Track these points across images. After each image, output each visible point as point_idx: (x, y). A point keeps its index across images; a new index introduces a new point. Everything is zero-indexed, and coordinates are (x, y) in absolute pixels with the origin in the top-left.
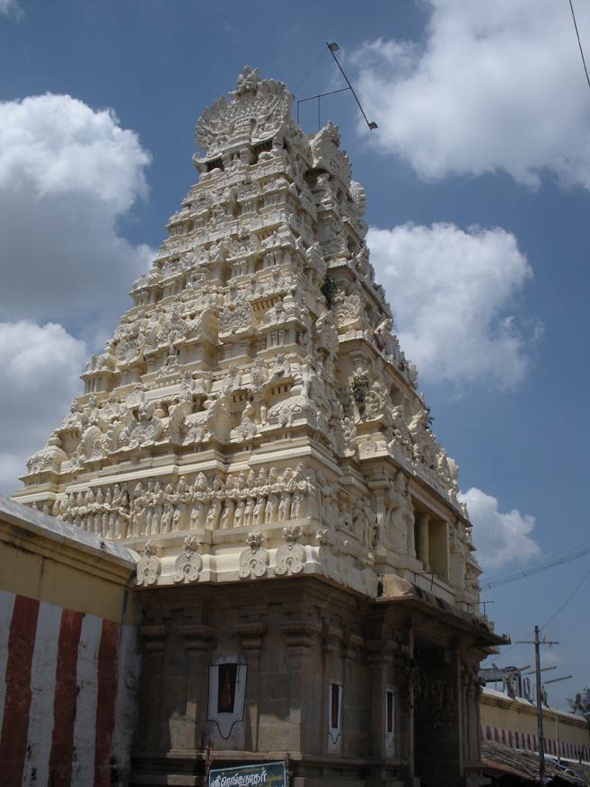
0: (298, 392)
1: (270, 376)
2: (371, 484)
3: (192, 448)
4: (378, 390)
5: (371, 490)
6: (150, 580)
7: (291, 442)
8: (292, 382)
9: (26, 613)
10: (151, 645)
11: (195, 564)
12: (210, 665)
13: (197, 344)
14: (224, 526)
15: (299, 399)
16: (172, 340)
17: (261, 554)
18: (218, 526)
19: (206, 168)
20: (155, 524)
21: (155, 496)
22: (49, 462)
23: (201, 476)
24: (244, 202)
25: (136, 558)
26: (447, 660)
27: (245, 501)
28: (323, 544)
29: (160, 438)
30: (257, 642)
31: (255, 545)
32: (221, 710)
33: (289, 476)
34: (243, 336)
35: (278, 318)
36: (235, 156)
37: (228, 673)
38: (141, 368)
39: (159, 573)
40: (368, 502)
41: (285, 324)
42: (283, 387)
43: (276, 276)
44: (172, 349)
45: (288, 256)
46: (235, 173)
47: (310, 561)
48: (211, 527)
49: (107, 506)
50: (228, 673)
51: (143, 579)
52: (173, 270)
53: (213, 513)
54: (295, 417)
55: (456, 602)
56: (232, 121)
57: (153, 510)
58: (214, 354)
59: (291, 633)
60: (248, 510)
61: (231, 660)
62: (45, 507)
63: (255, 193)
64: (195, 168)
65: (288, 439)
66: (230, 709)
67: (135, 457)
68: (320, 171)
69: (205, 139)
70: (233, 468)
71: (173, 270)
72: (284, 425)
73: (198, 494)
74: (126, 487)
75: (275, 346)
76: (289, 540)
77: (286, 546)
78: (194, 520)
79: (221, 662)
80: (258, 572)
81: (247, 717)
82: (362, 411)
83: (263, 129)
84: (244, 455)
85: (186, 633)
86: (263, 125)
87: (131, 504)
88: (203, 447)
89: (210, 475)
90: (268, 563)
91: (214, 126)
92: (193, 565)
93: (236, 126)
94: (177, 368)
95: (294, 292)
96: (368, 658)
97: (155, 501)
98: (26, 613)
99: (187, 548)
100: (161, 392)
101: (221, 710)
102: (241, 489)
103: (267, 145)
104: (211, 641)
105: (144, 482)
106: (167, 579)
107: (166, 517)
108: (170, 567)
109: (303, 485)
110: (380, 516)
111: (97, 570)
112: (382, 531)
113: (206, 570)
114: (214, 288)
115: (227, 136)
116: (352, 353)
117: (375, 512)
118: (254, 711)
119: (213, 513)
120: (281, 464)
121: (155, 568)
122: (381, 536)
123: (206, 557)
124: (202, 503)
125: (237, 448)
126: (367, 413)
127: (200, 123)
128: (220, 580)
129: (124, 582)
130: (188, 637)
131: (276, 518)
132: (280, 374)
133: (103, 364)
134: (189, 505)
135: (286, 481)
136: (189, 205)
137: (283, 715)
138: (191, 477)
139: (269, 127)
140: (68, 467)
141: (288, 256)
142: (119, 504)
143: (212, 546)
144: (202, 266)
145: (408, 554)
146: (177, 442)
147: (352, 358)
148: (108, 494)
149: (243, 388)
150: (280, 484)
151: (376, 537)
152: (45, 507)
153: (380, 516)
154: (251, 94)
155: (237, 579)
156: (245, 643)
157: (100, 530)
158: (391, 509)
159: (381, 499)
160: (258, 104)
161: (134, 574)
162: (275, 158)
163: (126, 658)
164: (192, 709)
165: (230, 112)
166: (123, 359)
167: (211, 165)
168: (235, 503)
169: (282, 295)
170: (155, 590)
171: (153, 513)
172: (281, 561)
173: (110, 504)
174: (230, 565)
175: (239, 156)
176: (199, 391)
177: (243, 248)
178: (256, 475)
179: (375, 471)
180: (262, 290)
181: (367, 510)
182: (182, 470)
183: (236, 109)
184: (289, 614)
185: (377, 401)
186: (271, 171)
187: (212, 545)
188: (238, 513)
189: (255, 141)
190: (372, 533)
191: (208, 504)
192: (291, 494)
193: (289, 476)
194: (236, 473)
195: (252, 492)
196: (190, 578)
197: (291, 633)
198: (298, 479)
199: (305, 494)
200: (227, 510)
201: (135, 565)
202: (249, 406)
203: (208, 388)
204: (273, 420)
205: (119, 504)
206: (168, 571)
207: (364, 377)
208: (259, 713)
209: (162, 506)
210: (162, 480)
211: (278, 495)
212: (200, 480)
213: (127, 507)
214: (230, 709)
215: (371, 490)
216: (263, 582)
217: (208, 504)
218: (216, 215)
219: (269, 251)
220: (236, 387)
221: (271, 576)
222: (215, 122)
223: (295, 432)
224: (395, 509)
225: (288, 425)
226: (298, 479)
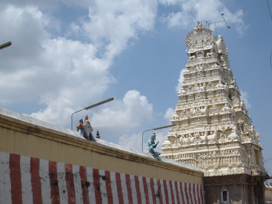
0: (233, 132)
1: (226, 127)
2: (247, 149)
3: (211, 145)
4: (246, 126)
5: (247, 150)
6: (207, 175)
7: (234, 145)
8: (231, 129)
9: (14, 162)
10: (207, 188)
11: (218, 172)
12: (220, 191)
13: (205, 117)
14: (221, 163)
15: (233, 135)
16: (198, 115)
17: (232, 170)
18: (220, 163)
19: (190, 55)
20: (205, 163)
21: (204, 156)
22: (169, 145)
23: (215, 152)
24: (207, 71)
25: (203, 171)
26: (260, 184)
27: (225, 157)
28: (244, 167)
29: (202, 142)
30: (231, 187)
31: (230, 168)
32: (224, 200)
33: (236, 153)
34: (216, 116)
35: (225, 112)
36: (200, 53)
37: (225, 193)
38: (189, 121)
39: (209, 174)
40: (247, 153)
41: (227, 114)
42: (229, 130)
43: (222, 99)
44: (198, 118)
45: (223, 92)
46: (200, 60)
47: (243, 171)
48: (218, 163)
49: (191, 158)
50: (225, 193)
51: (205, 175)
52: (190, 91)
53: (218, 160)
54: (235, 139)
55: (262, 170)
56: (196, 39)
57: (204, 159)
58: (209, 119)
59: (238, 185)
60: (226, 159)
61: (225, 190)
62: (172, 157)
63: (209, 69)
64: (187, 55)
65: (233, 144)
66: (226, 200)
67: (197, 147)
68: (221, 54)
69: (188, 44)
70: (221, 149)
71: (190, 91)
72: (232, 141)
73: (214, 156)
74: (196, 154)
75: (225, 119)
76: (238, 167)
77: (237, 168)
78: (214, 162)
79: (223, 191)
80: (232, 173)
81: (230, 202)
82: (243, 130)
83: (206, 44)
84: (223, 147)
85: (212, 185)
86: (206, 43)
87: (198, 158)
88: (213, 145)
89: (217, 152)
90: (234, 171)
91: (190, 40)
92: (217, 172)
93: (198, 42)
94: (201, 123)
95: (227, 104)
96: (249, 187)
97: (205, 158)
98: (14, 162)
99: (216, 169)
100: (198, 129)
101: (224, 200)
102: (224, 155)
103: (209, 51)
104: (221, 187)
105: (201, 153)
106: (211, 175)
107: (207, 161)
108: (212, 172)
109: (239, 155)
110: (249, 156)
111: (50, 138)
112: (250, 159)
113: (220, 173)
114: (205, 100)
115: (195, 45)
116: (238, 114)
117: (248, 155)
118: (232, 201)
119: (218, 160)
120: (234, 150)
121: (208, 173)
122: (250, 160)
123: (219, 170)
124: (216, 158)
125: (221, 144)
126: (244, 131)
127: (186, 39)
128: (223, 175)
129: (201, 176)
130: (216, 186)
131: (233, 162)
132: (229, 127)
133: (177, 118)
134: (212, 158)
135: (235, 154)
136: (188, 68)
137: (238, 201)
138: (212, 152)
139: (208, 44)
140: (174, 146)
141: (223, 92)
142: (194, 158)
143: (219, 167)
144: (200, 92)
145: (255, 163)
146: (207, 144)
147: (238, 115)
148: (191, 155)
149: (219, 129)
150: (234, 154)
151: (249, 161)
152: (172, 157)
153: (249, 156)
154: (200, 31)
155: (227, 175)
156: (229, 187)
157: (190, 163)
158: (251, 154)
159: (249, 152)
160: (203, 35)
161: (203, 174)
162: (212, 56)
163: (203, 192)
164: (218, 201)
165: (195, 36)
166: (183, 118)
167: (192, 55)
168: (223, 158)
169: (224, 104)
170: (208, 177)
171: (204, 160)
172: (236, 171)
173: (192, 157)
174: (225, 171)
175: (201, 53)
176: (209, 130)
177: (210, 88)
178: (228, 152)
179: (248, 146)
180: (218, 102)
181: (247, 155)
182: (210, 150)
183: (197, 36)
184: (238, 181)
185: (247, 128)
186: (212, 61)
187: (219, 167)
188: (224, 160)
189: (205, 49)
190: (248, 160)
191: (217, 158)
192: (236, 157)
193: (236, 153)
194: (222, 151)
195: (226, 155)
196: (217, 175)
197: (238, 185)
198: (238, 154)
199: (239, 156)
200: (221, 159)
201: (203, 172)
202: (221, 134)
203: (210, 129)
204: (229, 139)
205: (194, 158)
206: (211, 173)
207: (243, 122)
208: (233, 201)
209: (206, 159)
210: (206, 153)
211: (233, 157)
212: (214, 153)
213: (197, 158)
214: (226, 200)
215: (247, 150)
216: (233, 175)
217: (217, 158)
218: (199, 75)
219: (217, 90)
220: (217, 129)
221: (235, 174)
222: (190, 39)
223: (235, 142)
224: (252, 154)
225: (233, 141)
226: (238, 154)
